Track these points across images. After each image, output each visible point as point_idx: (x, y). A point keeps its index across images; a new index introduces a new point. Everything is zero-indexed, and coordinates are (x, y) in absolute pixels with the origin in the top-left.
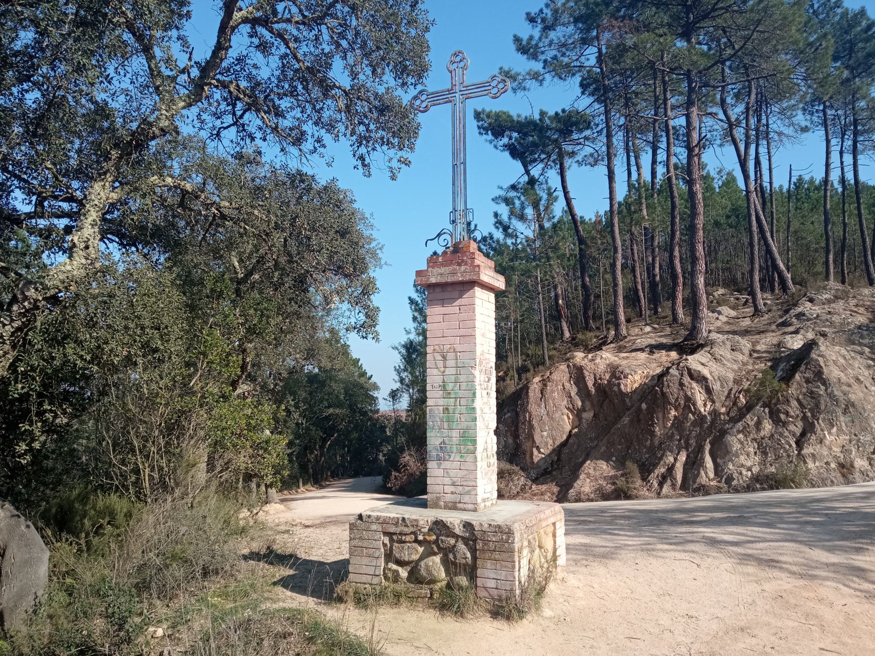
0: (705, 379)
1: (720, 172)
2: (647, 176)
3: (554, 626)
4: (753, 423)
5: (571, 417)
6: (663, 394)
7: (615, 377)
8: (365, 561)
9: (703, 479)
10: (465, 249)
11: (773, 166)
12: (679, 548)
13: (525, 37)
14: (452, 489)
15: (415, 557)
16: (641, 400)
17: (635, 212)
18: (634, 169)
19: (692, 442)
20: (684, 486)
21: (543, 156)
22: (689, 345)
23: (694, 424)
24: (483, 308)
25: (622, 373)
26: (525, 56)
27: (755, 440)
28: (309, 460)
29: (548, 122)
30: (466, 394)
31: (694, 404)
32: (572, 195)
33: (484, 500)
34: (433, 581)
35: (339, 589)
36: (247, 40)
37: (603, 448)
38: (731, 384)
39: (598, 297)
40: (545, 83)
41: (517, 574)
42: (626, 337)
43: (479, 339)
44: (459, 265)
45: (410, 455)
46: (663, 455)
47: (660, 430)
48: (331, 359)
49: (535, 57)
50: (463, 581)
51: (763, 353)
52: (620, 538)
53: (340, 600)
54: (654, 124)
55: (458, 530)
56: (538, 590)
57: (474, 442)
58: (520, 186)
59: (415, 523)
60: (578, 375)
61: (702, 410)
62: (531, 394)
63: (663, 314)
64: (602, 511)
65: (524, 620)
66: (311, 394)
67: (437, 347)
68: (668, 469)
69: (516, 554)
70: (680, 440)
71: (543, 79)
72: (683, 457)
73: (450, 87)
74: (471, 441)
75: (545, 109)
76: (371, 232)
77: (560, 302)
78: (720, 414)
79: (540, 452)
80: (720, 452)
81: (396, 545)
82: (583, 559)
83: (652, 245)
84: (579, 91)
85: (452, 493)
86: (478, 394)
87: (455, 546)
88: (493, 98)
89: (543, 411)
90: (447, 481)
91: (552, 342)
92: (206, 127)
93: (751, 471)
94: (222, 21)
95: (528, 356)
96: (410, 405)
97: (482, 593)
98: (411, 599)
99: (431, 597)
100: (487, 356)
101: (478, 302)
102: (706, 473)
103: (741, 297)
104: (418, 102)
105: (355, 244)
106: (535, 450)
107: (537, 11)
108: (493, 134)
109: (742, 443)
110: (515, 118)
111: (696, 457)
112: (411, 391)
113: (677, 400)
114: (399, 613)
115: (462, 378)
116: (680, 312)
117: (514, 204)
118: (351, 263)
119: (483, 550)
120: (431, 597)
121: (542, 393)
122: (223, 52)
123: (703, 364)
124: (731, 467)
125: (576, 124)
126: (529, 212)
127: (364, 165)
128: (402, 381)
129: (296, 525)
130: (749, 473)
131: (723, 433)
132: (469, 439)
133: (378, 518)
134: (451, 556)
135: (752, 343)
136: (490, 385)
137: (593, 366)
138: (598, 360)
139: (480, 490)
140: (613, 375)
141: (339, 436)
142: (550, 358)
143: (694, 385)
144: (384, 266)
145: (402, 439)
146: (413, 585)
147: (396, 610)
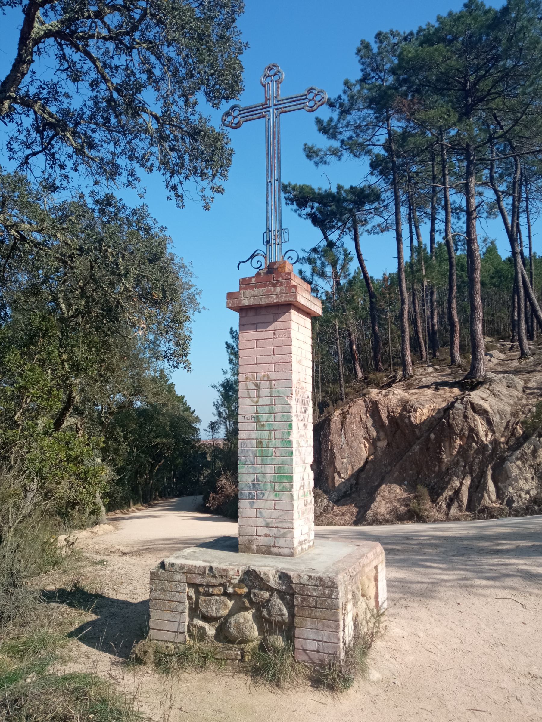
0: (486, 412)
1: (485, 241)
2: (425, 239)
3: (383, 695)
4: (530, 451)
5: (367, 446)
6: (450, 425)
7: (406, 410)
8: (168, 615)
9: (486, 501)
10: (280, 270)
11: (532, 234)
12: (497, 584)
13: (326, 119)
14: (266, 531)
15: (224, 612)
16: (429, 431)
17: (417, 271)
18: (415, 237)
19: (476, 467)
20: (470, 507)
21: (340, 224)
22: (470, 382)
23: (477, 452)
24: (300, 333)
25: (412, 407)
26: (326, 136)
27: (532, 466)
28: (139, 483)
29: (344, 194)
30: (281, 425)
31: (477, 435)
32: (364, 257)
33: (301, 543)
34: (245, 641)
35: (137, 648)
36: (54, 63)
37: (396, 474)
38: (508, 416)
39: (386, 343)
40: (343, 158)
41: (341, 635)
42: (412, 376)
43: (295, 367)
44: (274, 285)
45: (227, 479)
46: (450, 480)
47: (447, 458)
48: (155, 394)
49: (334, 136)
50: (279, 641)
51: (534, 389)
52: (434, 571)
53: (139, 661)
54: (432, 199)
55: (273, 582)
56: (363, 644)
57: (290, 479)
58: (320, 249)
59: (224, 574)
60: (373, 409)
61: (484, 439)
62: (333, 425)
63: (441, 358)
64: (408, 538)
65: (351, 691)
66: (141, 426)
67: (249, 375)
68: (455, 492)
69: (340, 612)
70: (464, 467)
71: (342, 155)
72: (467, 482)
73: (263, 102)
74: (287, 477)
75: (341, 184)
76: (190, 279)
77: (354, 347)
78: (500, 443)
79: (340, 477)
80: (501, 477)
81: (203, 598)
82: (401, 598)
83: (431, 299)
84: (368, 169)
85: (266, 536)
86: (294, 426)
87: (269, 600)
88: (310, 111)
89: (343, 440)
90: (260, 522)
91: (347, 382)
92: (16, 156)
93: (529, 494)
94: (22, 31)
95: (327, 393)
96: (227, 436)
97: (301, 657)
98: (219, 661)
99: (242, 660)
100: (304, 385)
101: (294, 326)
102: (489, 496)
103: (506, 343)
104: (230, 118)
105: (163, 270)
106: (336, 475)
107: (336, 96)
108: (297, 205)
109: (520, 469)
110: (317, 191)
111: (479, 482)
112: (228, 423)
113: (461, 430)
114: (205, 680)
115: (277, 408)
116: (457, 354)
117: (315, 263)
118: (164, 293)
119: (302, 607)
120: (242, 660)
121: (342, 425)
122: (25, 66)
123: (483, 399)
124: (511, 490)
125: (367, 196)
126: (329, 270)
127: (177, 196)
128: (220, 414)
129: (114, 552)
130: (528, 496)
131: (504, 460)
132: (284, 476)
133: (182, 567)
134: (265, 612)
135: (524, 380)
136: (306, 415)
137: (386, 401)
138: (391, 396)
139: (297, 533)
140: (404, 409)
141: (166, 461)
142: (347, 394)
143: (477, 417)
144: (202, 311)
145: (219, 464)
146: (220, 645)
147: (201, 675)
